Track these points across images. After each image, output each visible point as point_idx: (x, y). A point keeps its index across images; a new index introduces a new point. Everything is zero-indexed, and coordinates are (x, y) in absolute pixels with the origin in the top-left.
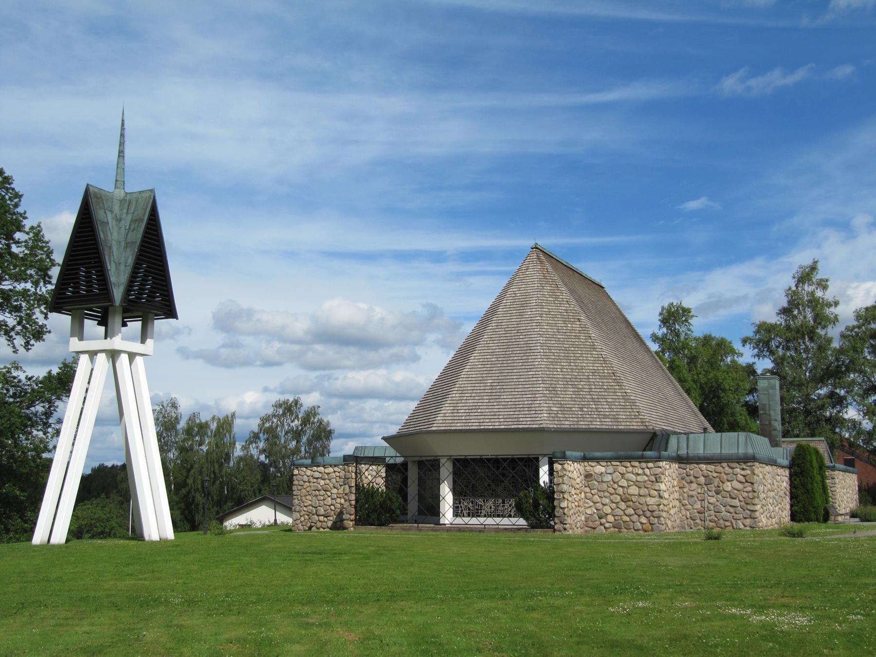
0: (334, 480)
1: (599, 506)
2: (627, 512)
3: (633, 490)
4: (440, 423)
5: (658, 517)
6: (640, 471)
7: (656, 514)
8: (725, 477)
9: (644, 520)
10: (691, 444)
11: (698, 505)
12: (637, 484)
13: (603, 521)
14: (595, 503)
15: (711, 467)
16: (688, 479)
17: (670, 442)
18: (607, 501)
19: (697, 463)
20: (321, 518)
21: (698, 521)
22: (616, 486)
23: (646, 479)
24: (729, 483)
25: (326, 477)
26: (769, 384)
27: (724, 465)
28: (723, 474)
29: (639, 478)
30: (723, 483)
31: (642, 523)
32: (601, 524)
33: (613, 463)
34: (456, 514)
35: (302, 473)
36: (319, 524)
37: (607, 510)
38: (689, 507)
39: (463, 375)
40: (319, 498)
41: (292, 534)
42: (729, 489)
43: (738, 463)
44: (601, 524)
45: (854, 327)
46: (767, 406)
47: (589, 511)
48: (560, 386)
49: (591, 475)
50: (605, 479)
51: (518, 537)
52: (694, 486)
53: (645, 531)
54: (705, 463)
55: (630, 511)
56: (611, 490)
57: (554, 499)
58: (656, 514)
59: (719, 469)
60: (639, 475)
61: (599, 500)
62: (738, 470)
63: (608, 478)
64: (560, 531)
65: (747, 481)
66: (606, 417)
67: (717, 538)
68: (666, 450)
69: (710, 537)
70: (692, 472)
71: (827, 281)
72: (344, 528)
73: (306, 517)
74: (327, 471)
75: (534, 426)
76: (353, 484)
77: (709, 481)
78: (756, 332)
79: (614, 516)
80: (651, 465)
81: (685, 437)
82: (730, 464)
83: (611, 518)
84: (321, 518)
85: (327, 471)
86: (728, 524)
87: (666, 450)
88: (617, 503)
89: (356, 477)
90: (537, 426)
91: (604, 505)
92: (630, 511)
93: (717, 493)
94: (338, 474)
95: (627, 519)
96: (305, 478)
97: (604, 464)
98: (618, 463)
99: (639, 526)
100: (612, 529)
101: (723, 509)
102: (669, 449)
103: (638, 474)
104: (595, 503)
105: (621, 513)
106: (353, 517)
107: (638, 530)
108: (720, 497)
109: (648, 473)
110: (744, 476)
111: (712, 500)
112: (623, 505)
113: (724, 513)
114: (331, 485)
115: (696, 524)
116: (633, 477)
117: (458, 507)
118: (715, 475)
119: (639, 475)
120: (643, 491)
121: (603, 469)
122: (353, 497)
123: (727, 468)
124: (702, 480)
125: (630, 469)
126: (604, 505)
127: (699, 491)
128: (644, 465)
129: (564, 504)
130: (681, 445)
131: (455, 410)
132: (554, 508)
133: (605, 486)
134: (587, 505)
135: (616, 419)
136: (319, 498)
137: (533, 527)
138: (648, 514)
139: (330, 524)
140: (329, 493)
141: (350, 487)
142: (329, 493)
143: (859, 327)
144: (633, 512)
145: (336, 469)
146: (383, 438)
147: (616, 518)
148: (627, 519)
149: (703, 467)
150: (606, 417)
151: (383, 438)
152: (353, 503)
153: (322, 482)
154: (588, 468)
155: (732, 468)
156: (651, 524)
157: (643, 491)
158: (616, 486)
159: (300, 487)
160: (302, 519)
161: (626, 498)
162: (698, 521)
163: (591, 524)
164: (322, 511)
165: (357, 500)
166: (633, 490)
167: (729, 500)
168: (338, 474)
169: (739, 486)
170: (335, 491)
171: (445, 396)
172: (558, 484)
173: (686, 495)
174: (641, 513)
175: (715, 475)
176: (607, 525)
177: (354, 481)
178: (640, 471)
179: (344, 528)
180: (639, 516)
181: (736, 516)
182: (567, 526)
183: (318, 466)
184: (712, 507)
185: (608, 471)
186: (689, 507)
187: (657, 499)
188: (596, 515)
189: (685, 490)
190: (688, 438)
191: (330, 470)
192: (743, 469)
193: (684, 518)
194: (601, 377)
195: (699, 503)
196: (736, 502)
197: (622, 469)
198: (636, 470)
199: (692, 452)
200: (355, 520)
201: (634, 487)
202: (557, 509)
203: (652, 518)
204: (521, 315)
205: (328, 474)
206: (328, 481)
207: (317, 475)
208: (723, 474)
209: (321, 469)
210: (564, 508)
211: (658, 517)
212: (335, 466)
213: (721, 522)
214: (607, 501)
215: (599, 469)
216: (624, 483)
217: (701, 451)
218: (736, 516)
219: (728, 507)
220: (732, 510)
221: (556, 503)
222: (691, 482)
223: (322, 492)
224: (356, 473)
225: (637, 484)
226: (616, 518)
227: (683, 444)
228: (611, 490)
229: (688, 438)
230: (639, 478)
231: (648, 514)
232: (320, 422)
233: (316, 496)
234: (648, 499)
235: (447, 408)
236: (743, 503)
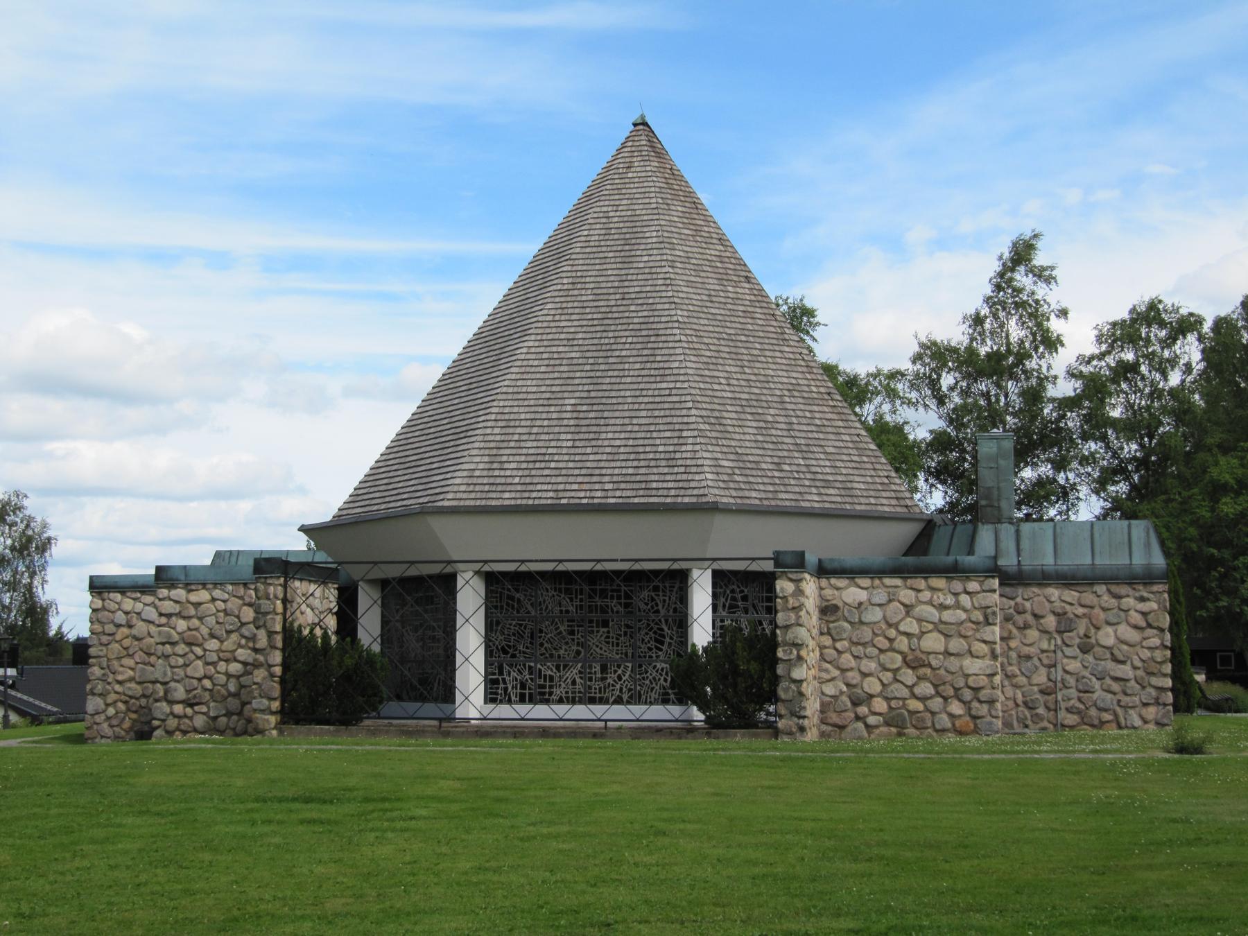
0: (211, 621)
1: (854, 677)
2: (917, 690)
3: (933, 642)
4: (458, 487)
5: (991, 702)
6: (950, 600)
7: (984, 694)
8: (1102, 615)
9: (956, 708)
10: (1025, 544)
11: (1041, 678)
12: (941, 627)
13: (863, 710)
14: (843, 671)
15: (1071, 595)
16: (1020, 619)
17: (978, 540)
18: (872, 666)
19: (1040, 585)
20: (178, 709)
21: (1041, 711)
22: (892, 633)
23: (964, 616)
24: (1110, 630)
25: (192, 612)
26: (999, 448)
27: (1101, 589)
28: (1097, 610)
29: (947, 616)
30: (1098, 628)
31: (951, 716)
32: (858, 718)
33: (888, 581)
34: (491, 697)
35: (113, 606)
36: (172, 723)
37: (872, 686)
38: (1022, 680)
39: (505, 384)
40: (173, 661)
41: (85, 748)
42: (1110, 641)
43: (1129, 584)
44: (858, 718)
45: (1092, 358)
46: (995, 492)
47: (830, 690)
48: (730, 416)
49: (836, 608)
50: (868, 617)
51: (693, 747)
52: (1033, 634)
53: (961, 733)
54: (1057, 586)
55: (926, 689)
56: (882, 642)
57: (775, 661)
58: (984, 694)
59: (1089, 598)
60: (947, 608)
61: (853, 663)
62: (1129, 602)
63: (875, 615)
64: (790, 733)
65: (1150, 626)
66: (828, 484)
67: (1198, 750)
68: (971, 552)
69: (1181, 749)
70: (1028, 605)
71: (1052, 268)
72: (259, 731)
73: (121, 706)
74: (194, 597)
75: (686, 500)
76: (278, 628)
77: (1065, 624)
78: (917, 358)
79: (887, 699)
80: (973, 586)
81: (1012, 529)
82: (1114, 588)
83: (880, 705)
84: (178, 709)
85: (194, 597)
86: (1107, 717)
87: (971, 552)
88: (895, 671)
89: (285, 609)
90: (694, 500)
91: (865, 675)
92: (926, 689)
93: (1085, 649)
94: (221, 605)
95: (919, 706)
96: (120, 617)
97: (865, 582)
98: (898, 582)
99: (944, 721)
100: (884, 729)
101: (1097, 685)
102: (977, 553)
103: (942, 607)
104: (843, 671)
105: (905, 692)
106: (276, 705)
107: (944, 730)
108: (1090, 658)
109: (968, 604)
110: (1144, 614)
111: (1073, 666)
112: (908, 676)
113: (1098, 694)
114: (205, 631)
115: (1037, 718)
116: (933, 614)
117: (496, 682)
118: (1080, 611)
119: (947, 608)
120: (956, 645)
121: (863, 596)
122: (277, 657)
123: (1106, 597)
124: (1050, 622)
125: (926, 595)
126: (865, 675)
127: (1045, 646)
128: (957, 586)
129: (797, 674)
130: (1003, 545)
131: (495, 462)
132: (776, 679)
133: (867, 634)
134: (825, 676)
135: (847, 490)
136: (173, 661)
137: (714, 725)
138: (967, 694)
139: (199, 721)
140: (199, 651)
141: (271, 634)
142: (199, 651)
143: (1101, 356)
144: (931, 691)
145: (217, 593)
146: (303, 529)
147: (893, 704)
148: (919, 706)
149: (1054, 592)
150: (828, 484)
151: (303, 529)
152: (278, 670)
153: (182, 625)
154: (828, 593)
155: (1118, 597)
156: (975, 718)
157: (956, 645)
158: (892, 633)
159: (105, 639)
160: (111, 711)
161: (917, 659)
162: (1041, 711)
163: (834, 718)
164: (180, 692)
165: (285, 665)
166: (933, 642)
167: (1110, 665)
168: (221, 605)
169: (1133, 636)
170: (213, 644)
171: (462, 434)
172: (787, 627)
173: (1013, 655)
174: (951, 692)
175: (1080, 611)
176: (872, 720)
177: (279, 618)
178: (950, 600)
179: (259, 731)
180: (945, 699)
181: (1125, 700)
182: (806, 722)
183: (172, 586)
184: (1071, 681)
185: (876, 600)
186: (1022, 680)
187: (988, 662)
188: (845, 698)
189: (1013, 644)
190: (1018, 532)
191: (203, 595)
192: (1142, 599)
193: (1011, 704)
194: (809, 401)
195: (1043, 671)
196: (1125, 671)
197: (907, 596)
198: (941, 598)
199: (1028, 563)
200: (282, 712)
201: (935, 634)
202: (783, 684)
203: (975, 704)
204: (627, 261)
205: (197, 605)
206: (196, 622)
207: (168, 607)
208: (1097, 610)
209: (179, 593)
210: (801, 681)
211: (991, 702)
212: (215, 585)
213: (1093, 712)
214: (872, 666)
215: (852, 593)
216: (910, 626)
217: (1049, 560)
218: (1125, 700)
219: (1108, 681)
220: (1116, 687)
221: (780, 670)
222: (1026, 626)
223: (181, 649)
224: (285, 601)
225: (941, 627)
226: (893, 704)
227: (1008, 544)
228: (882, 642)
229: (1018, 532)
230: (947, 616)
231: (967, 694)
232: (29, 520)
233: (167, 657)
234: (967, 662)
235: (474, 459)
236: (1140, 673)
